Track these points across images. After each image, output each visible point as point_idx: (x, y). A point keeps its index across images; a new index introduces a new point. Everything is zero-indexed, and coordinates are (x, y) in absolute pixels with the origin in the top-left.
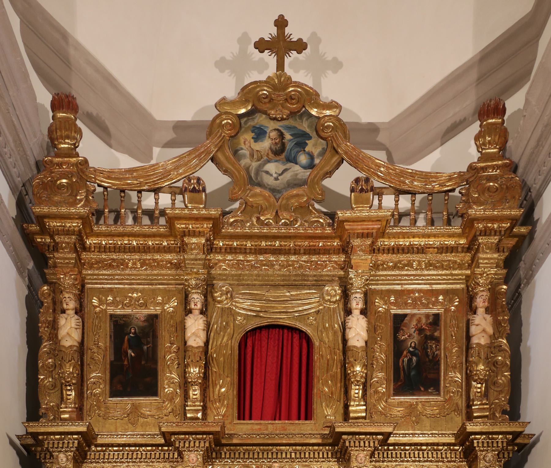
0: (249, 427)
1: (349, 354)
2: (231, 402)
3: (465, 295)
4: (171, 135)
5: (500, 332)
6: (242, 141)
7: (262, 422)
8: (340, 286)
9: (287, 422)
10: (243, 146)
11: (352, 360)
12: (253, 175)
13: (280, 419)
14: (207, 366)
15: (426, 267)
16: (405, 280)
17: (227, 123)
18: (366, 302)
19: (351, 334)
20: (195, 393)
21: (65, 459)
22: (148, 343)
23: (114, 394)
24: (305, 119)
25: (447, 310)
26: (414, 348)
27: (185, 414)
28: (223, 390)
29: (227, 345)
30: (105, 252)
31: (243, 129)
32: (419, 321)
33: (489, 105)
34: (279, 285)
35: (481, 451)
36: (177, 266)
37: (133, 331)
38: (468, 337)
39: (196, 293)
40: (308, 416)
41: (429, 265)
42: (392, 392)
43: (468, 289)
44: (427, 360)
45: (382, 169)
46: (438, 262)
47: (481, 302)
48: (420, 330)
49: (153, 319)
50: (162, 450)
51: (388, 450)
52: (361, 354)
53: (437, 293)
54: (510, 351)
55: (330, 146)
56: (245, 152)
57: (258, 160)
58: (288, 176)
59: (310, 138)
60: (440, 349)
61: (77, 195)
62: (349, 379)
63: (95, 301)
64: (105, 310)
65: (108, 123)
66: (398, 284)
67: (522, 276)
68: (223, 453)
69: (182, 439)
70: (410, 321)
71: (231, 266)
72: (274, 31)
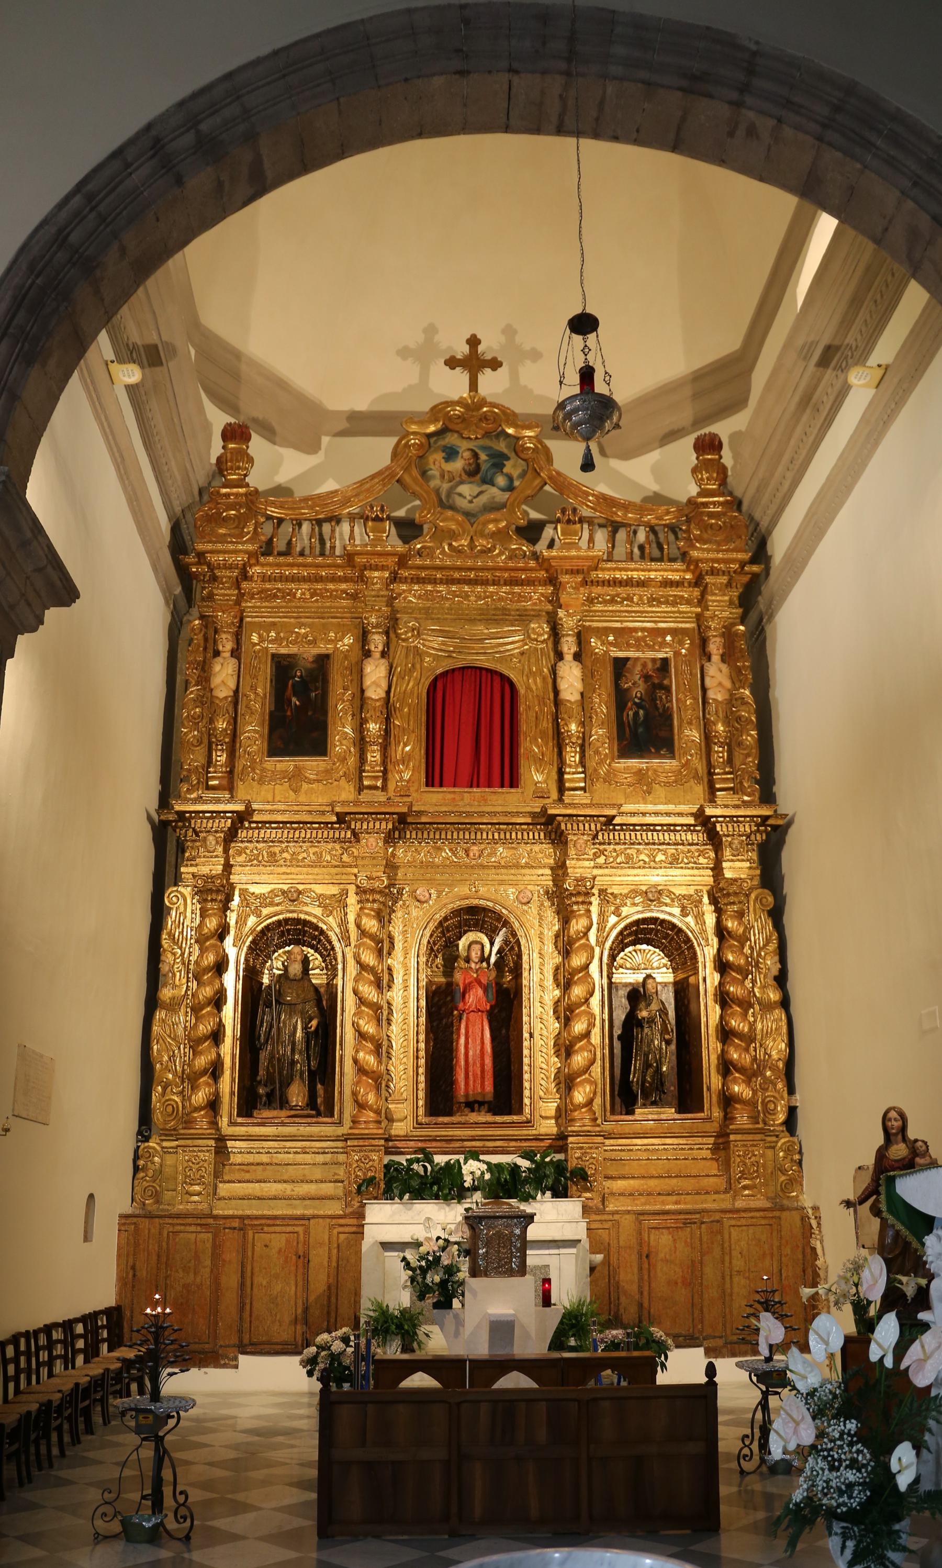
0: (440, 796)
1: (562, 708)
2: (417, 764)
3: (697, 636)
4: (343, 425)
5: (741, 681)
6: (431, 460)
7: (457, 789)
8: (548, 622)
9: (487, 790)
10: (432, 466)
11: (566, 717)
12: (443, 497)
13: (478, 786)
14: (388, 720)
15: (649, 602)
16: (626, 617)
17: (415, 443)
18: (579, 643)
19: (563, 685)
20: (374, 756)
21: (214, 843)
22: (317, 689)
23: (273, 752)
24: (502, 439)
25: (677, 654)
26: (640, 698)
27: (361, 779)
28: (408, 748)
29: (412, 692)
30: (270, 581)
31: (432, 449)
32: (644, 665)
33: (703, 440)
34: (475, 619)
35: (725, 835)
36: (354, 597)
37: (298, 674)
38: (704, 690)
39: (377, 633)
40: (513, 780)
41: (652, 600)
42: (616, 754)
43: (699, 629)
44: (657, 713)
45: (591, 498)
46: (662, 596)
47: (715, 647)
48: (646, 677)
49: (323, 660)
50: (332, 828)
51: (615, 830)
52: (576, 709)
53: (663, 632)
54: (756, 703)
55: (530, 467)
56: (435, 472)
57: (450, 481)
58: (483, 499)
59: (508, 459)
60: (671, 701)
61: (244, 528)
62: (564, 740)
63: (255, 638)
64: (267, 648)
65: (274, 424)
66: (617, 621)
67: (764, 610)
68: (408, 832)
69: (359, 820)
70: (634, 666)
71: (420, 597)
72: (466, 349)
